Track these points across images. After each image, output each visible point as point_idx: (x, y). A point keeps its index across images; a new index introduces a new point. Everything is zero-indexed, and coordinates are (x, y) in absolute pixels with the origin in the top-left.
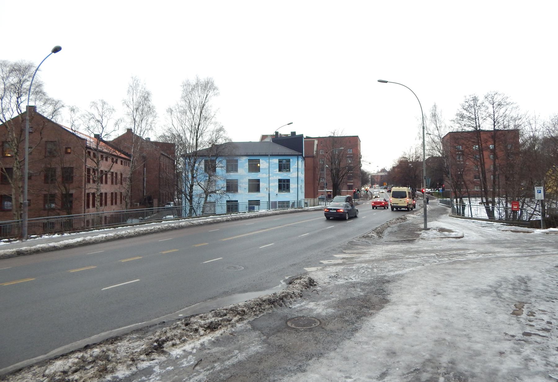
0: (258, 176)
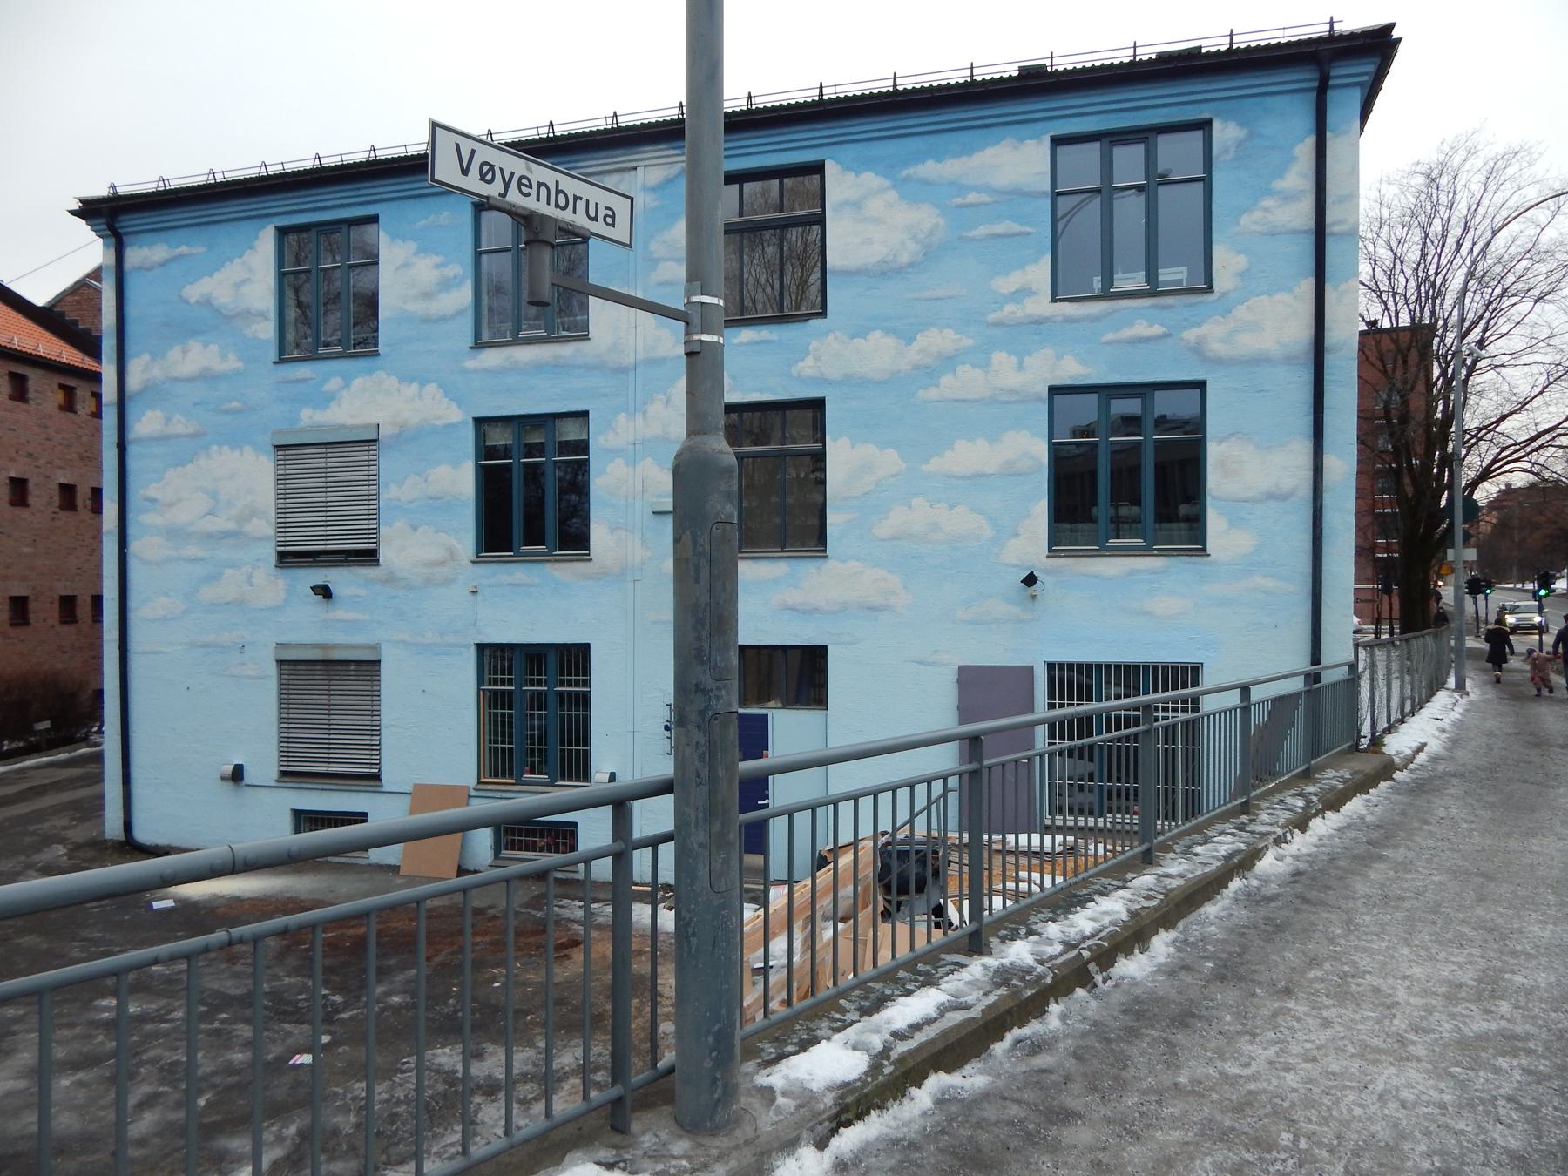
0: (807, 367)
